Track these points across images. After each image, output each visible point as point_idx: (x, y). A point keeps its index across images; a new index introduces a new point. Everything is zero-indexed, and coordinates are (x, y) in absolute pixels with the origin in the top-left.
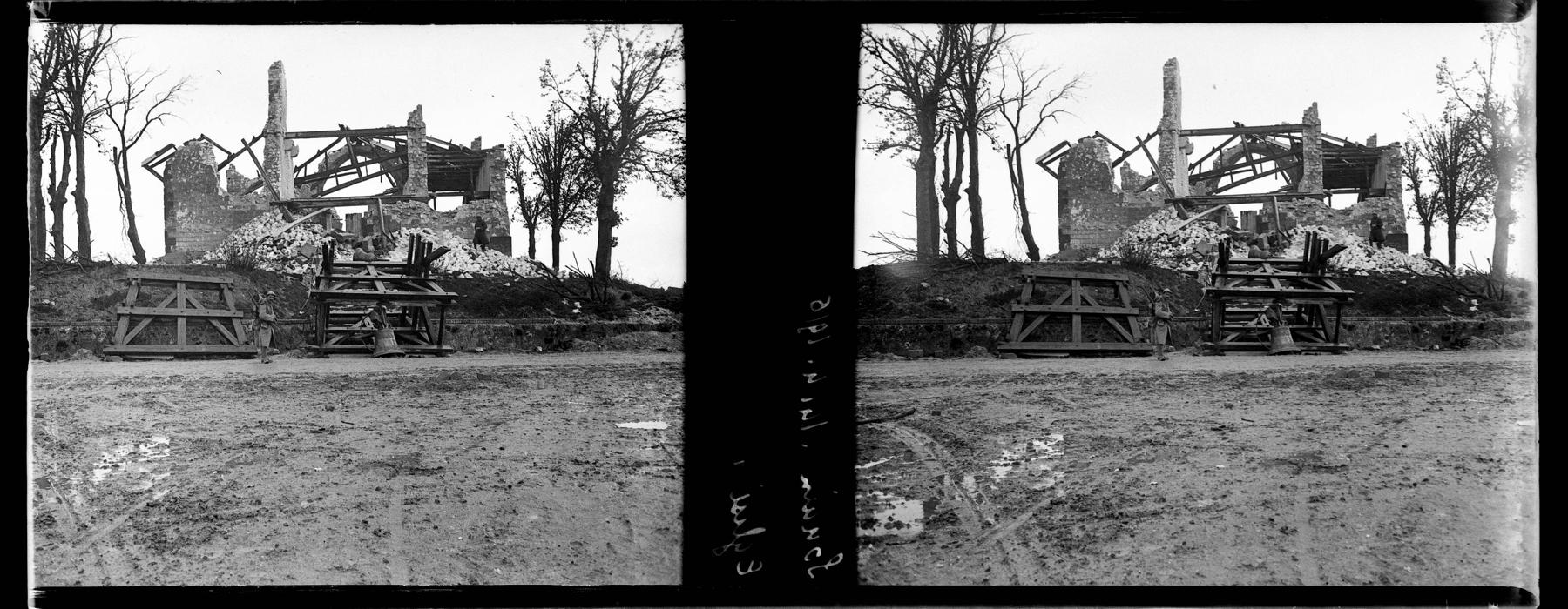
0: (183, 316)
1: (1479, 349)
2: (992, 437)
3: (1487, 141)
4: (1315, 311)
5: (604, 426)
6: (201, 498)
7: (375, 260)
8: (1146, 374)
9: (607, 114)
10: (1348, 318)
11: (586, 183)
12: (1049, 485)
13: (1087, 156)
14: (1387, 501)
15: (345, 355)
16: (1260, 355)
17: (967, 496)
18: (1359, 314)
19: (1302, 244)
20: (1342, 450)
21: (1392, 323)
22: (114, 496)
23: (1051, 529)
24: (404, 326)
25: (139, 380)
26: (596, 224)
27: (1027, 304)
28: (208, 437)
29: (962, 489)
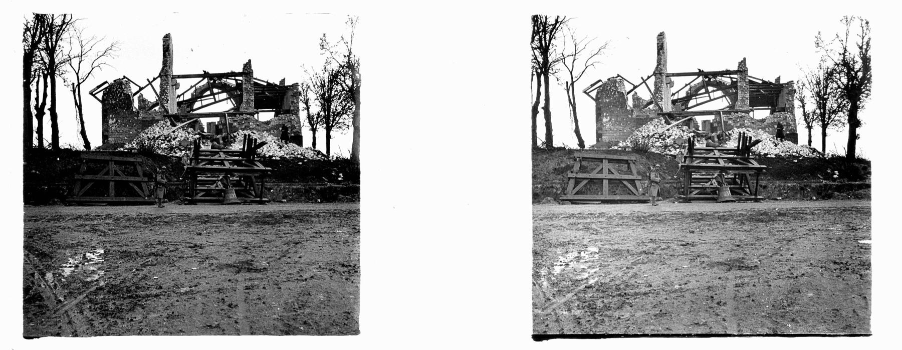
0: (606, 179)
1: (343, 202)
2: (554, 249)
3: (349, 82)
4: (744, 178)
5: (852, 242)
6: (617, 283)
7: (224, 148)
8: (645, 213)
9: (854, 63)
10: (268, 184)
11: (841, 102)
12: (95, 279)
13: (119, 90)
14: (289, 289)
15: (700, 201)
16: (217, 205)
17: (48, 285)
18: (274, 182)
19: (242, 141)
20: (755, 257)
21: (293, 187)
22: (77, 283)
23: (584, 302)
24: (736, 185)
25: (581, 215)
26: (847, 126)
27: (577, 173)
28: (621, 248)
29: (45, 281)
